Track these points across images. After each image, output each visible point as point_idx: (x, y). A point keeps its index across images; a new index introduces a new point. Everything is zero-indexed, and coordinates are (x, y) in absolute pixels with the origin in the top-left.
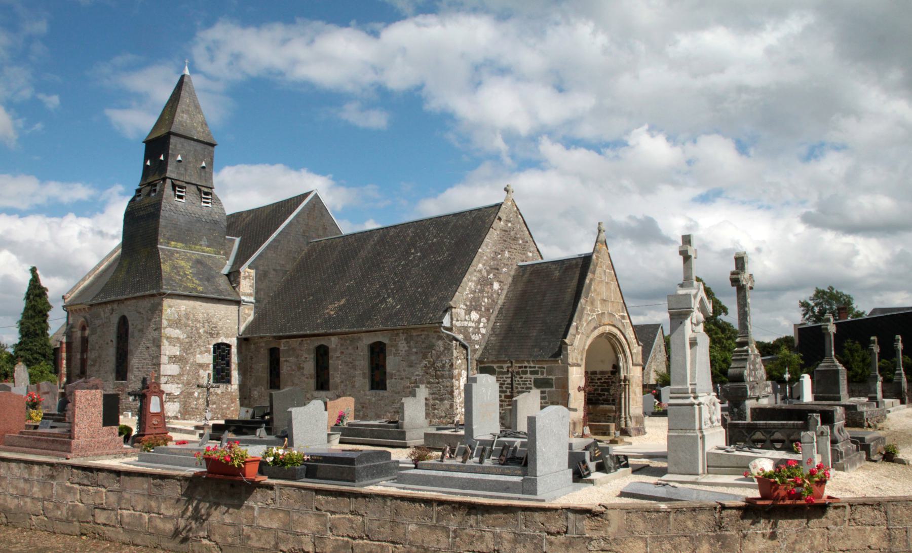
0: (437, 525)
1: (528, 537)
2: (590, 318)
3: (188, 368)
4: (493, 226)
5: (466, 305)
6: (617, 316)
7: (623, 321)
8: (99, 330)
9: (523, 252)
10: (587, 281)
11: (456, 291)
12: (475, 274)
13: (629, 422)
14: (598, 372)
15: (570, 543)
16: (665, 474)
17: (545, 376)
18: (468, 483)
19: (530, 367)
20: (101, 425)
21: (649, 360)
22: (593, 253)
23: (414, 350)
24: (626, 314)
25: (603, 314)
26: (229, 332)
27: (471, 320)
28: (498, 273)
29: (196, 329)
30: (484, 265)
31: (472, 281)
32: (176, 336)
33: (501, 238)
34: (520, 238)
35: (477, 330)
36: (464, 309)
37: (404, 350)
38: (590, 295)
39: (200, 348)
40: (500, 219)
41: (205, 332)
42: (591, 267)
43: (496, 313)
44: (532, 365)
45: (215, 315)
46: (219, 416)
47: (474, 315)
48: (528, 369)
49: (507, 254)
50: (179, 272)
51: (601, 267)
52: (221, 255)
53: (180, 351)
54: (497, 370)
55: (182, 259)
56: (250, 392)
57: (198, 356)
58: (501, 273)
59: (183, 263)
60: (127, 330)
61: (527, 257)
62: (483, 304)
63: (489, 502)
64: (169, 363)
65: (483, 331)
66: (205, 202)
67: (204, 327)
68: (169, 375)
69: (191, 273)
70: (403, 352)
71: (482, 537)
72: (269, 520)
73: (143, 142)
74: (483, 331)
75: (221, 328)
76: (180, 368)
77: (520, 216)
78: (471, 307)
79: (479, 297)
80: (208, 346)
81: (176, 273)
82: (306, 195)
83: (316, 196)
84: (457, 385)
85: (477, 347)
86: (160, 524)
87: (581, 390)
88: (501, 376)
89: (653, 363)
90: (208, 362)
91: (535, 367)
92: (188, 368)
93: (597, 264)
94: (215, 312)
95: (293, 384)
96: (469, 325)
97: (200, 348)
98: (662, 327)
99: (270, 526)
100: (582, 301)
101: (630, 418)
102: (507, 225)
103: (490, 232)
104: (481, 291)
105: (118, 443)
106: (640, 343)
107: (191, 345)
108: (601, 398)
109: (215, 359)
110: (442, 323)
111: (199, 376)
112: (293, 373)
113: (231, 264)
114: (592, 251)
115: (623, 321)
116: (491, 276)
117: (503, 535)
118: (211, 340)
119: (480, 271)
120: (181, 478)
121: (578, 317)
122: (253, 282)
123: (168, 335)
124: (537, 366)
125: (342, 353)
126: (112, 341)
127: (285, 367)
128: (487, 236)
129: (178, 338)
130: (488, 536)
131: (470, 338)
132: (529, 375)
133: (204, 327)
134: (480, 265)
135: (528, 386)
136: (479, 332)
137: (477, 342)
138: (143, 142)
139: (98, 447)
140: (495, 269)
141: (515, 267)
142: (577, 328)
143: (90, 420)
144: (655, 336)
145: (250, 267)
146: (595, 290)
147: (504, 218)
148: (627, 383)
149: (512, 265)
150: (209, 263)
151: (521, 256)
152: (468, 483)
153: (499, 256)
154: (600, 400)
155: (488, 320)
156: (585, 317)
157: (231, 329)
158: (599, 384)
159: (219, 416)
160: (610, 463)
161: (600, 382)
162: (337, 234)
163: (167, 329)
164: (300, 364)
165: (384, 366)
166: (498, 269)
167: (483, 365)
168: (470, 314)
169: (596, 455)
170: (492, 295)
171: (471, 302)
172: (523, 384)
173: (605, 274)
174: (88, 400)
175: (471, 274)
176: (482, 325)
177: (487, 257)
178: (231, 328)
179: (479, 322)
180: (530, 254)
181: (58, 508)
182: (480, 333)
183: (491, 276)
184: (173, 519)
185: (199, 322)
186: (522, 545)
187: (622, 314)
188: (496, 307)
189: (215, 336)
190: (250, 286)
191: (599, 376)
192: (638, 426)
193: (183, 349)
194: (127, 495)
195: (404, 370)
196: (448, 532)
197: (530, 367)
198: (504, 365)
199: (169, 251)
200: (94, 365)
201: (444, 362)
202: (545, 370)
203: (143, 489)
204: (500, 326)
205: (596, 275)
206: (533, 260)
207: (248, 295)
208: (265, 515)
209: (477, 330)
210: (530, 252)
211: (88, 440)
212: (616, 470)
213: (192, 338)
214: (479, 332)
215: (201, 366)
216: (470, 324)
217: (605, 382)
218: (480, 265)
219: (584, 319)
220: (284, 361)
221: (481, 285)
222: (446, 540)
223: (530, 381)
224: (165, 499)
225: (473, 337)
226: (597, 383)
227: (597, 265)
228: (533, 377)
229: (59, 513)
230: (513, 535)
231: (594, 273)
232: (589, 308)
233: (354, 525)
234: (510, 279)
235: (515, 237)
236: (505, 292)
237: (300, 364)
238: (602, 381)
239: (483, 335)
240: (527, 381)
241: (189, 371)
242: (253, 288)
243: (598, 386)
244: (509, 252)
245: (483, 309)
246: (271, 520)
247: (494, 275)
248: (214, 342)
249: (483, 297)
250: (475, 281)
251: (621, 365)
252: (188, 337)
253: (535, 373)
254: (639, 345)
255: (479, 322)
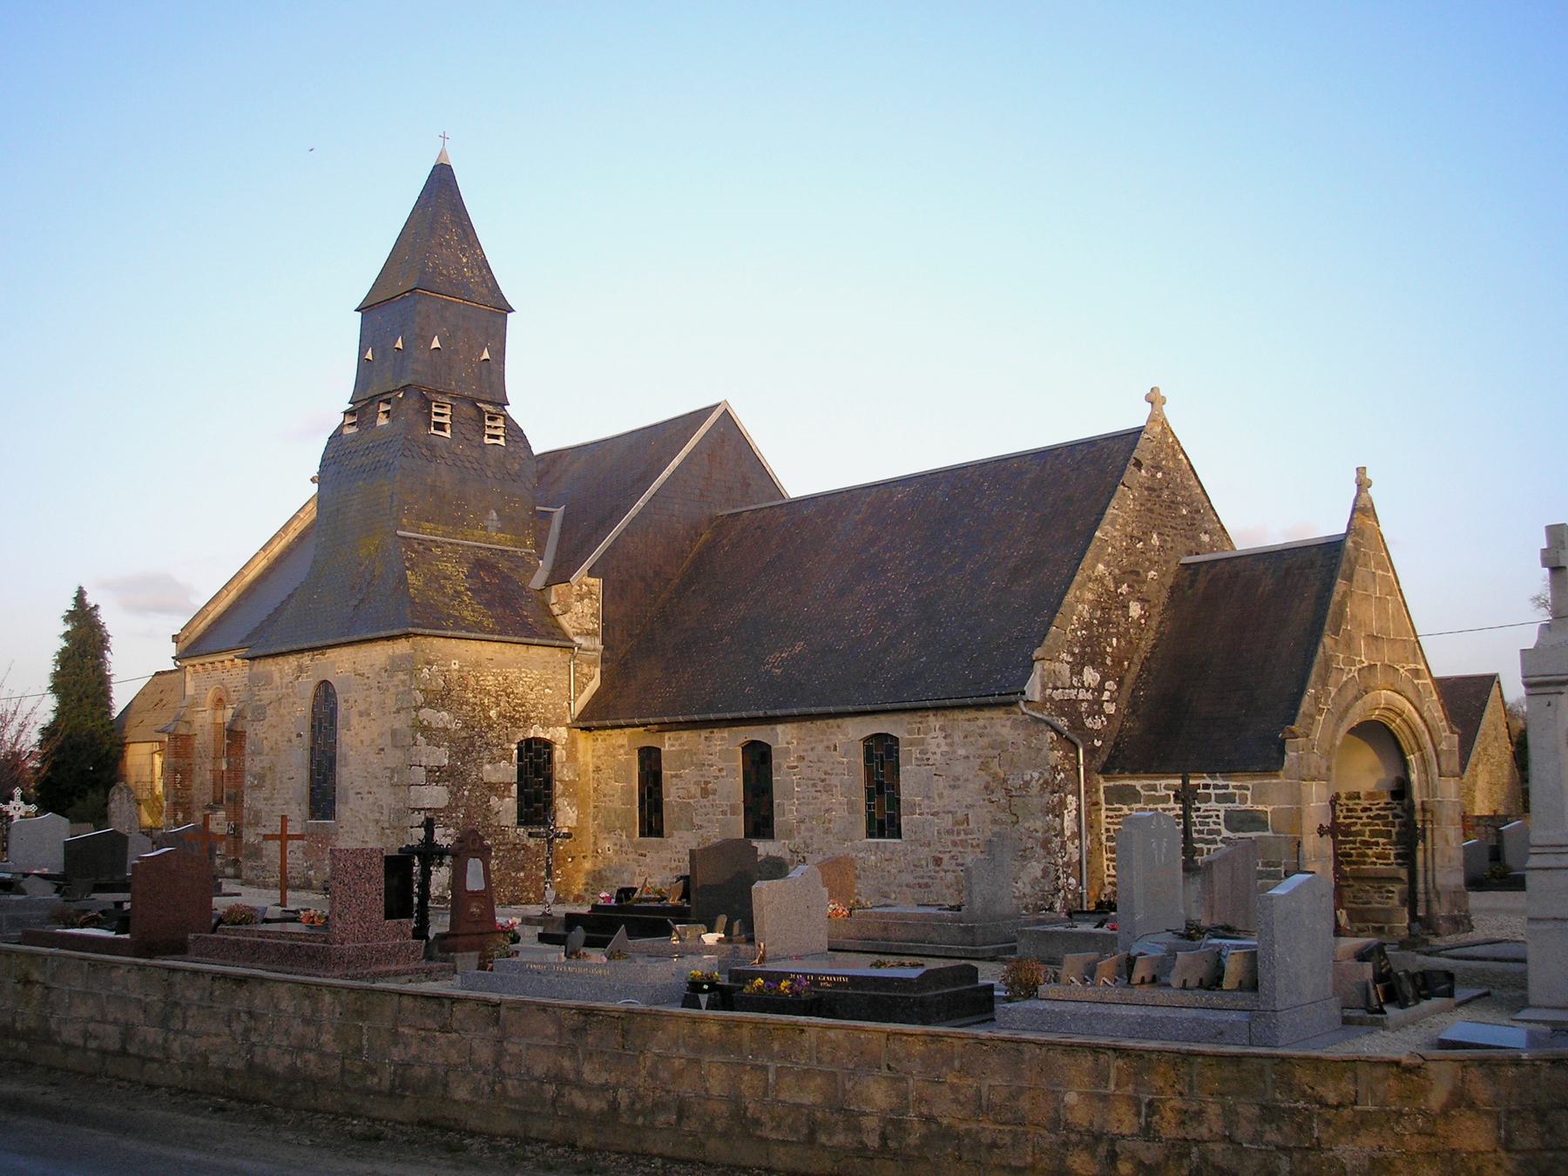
0: (1117, 1092)
1: (1284, 1112)
2: (1345, 679)
3: (466, 793)
4: (1124, 479)
5: (1073, 654)
6: (1402, 670)
7: (1416, 682)
8: (269, 712)
9: (1190, 533)
10: (1336, 597)
11: (1050, 624)
12: (1090, 585)
13: (1436, 907)
14: (1362, 795)
15: (1362, 1122)
16: (1523, 1007)
17: (1248, 805)
18: (1140, 1024)
19: (1216, 787)
20: (382, 916)
21: (1473, 759)
22: (1346, 535)
23: (962, 752)
24: (1422, 667)
25: (1372, 667)
26: (549, 715)
27: (1083, 686)
28: (1137, 582)
29: (483, 710)
30: (1107, 565)
31: (1083, 602)
32: (441, 725)
33: (1141, 505)
34: (1183, 503)
35: (1096, 707)
36: (1068, 663)
37: (938, 751)
38: (1343, 627)
39: (490, 750)
40: (1138, 464)
41: (500, 715)
42: (1344, 566)
43: (1136, 669)
44: (1220, 782)
45: (521, 679)
46: (531, 895)
47: (1091, 676)
48: (1211, 791)
49: (1155, 540)
50: (443, 587)
51: (1366, 565)
52: (526, 547)
53: (450, 757)
54: (1142, 792)
55: (449, 560)
56: (595, 843)
57: (488, 767)
58: (1144, 582)
59: (449, 568)
60: (334, 711)
61: (1200, 544)
62: (1108, 649)
63: (1215, 1050)
64: (428, 782)
65: (1110, 708)
66: (491, 436)
67: (498, 705)
68: (430, 809)
69: (468, 589)
70: (938, 756)
71: (1201, 1112)
72: (796, 1090)
73: (357, 310)
74: (1110, 708)
75: (534, 705)
76: (451, 792)
77: (1181, 456)
78: (1082, 658)
79: (1099, 636)
80: (506, 746)
81: (436, 590)
82: (699, 416)
83: (727, 417)
84: (1058, 828)
85: (1098, 743)
86: (580, 1101)
87: (1326, 833)
88: (1151, 806)
89: (1480, 767)
90: (507, 780)
91: (1226, 787)
92: (466, 793)
93: (1356, 558)
94: (521, 672)
95: (693, 825)
96: (1080, 697)
97: (490, 750)
98: (1499, 682)
99: (798, 1101)
100: (1327, 640)
101: (1438, 894)
102: (1153, 475)
103: (1118, 494)
104: (1104, 622)
105: (412, 953)
106: (1455, 729)
107: (473, 745)
108: (1370, 852)
109: (521, 772)
110: (1023, 693)
111: (488, 809)
112: (691, 801)
113: (549, 566)
114: (1344, 531)
115: (1416, 682)
116: (1124, 588)
117: (1240, 1109)
118: (514, 734)
119: (1100, 580)
120: (623, 1015)
121: (1319, 676)
122: (599, 605)
123: (425, 723)
124: (1232, 783)
125: (802, 758)
126: (299, 735)
127: (673, 790)
128: (1113, 502)
129: (446, 729)
130: (1213, 1110)
131: (1084, 724)
132: (1213, 804)
133: (498, 705)
134: (1101, 567)
135: (1213, 827)
136: (1101, 712)
137: (1098, 734)
138: (357, 310)
139: (377, 959)
140: (1132, 572)
141: (1173, 567)
142: (1317, 699)
143: (362, 908)
144: (1485, 704)
145: (591, 573)
146: (1354, 616)
147: (1146, 462)
148: (1429, 815)
149: (1166, 562)
150: (503, 565)
151: (1187, 542)
152: (1140, 1024)
153: (1140, 545)
154: (1367, 856)
155: (1120, 684)
156: (1334, 675)
157: (555, 709)
158: (1365, 820)
159: (531, 895)
160: (1408, 989)
161: (1368, 817)
162: (773, 498)
163: (422, 711)
164: (707, 783)
165: (895, 786)
166: (1138, 574)
167: (1111, 784)
168: (1080, 673)
169: (1384, 970)
170: (1127, 630)
171: (1083, 647)
172: (1201, 824)
173: (1374, 580)
174: (358, 867)
175: (1081, 586)
176: (1106, 695)
177: (1113, 548)
178: (554, 704)
179: (1100, 688)
180: (1205, 538)
181: (373, 1072)
182: (1104, 713)
183: (1124, 588)
184: (608, 1090)
185: (488, 693)
186: (1274, 1126)
187: (1412, 666)
188: (1136, 657)
189: (521, 724)
190: (592, 615)
191: (1366, 804)
192: (1456, 913)
193: (456, 753)
194: (512, 1048)
195: (941, 796)
196: (1138, 1106)
197: (1216, 787)
198: (1158, 783)
199: (421, 542)
200: (260, 787)
201: (1027, 778)
202: (1249, 793)
203: (546, 1036)
204: (1145, 696)
205: (1355, 584)
206: (1212, 551)
207: (588, 634)
208: (790, 1080)
209: (1096, 708)
210: (1206, 533)
211: (359, 945)
212: (1417, 1002)
213: (474, 728)
214: (1101, 712)
215: (492, 787)
216: (1083, 695)
217: (1377, 817)
218: (1101, 567)
219: (1331, 680)
220: (672, 776)
221: (1103, 609)
222: (1135, 1120)
223: (1217, 816)
224: (591, 1054)
225: (1089, 723)
226: (1361, 818)
227: (1356, 562)
228: (1223, 807)
229: (376, 1080)
230: (1257, 1107)
231: (1349, 578)
232: (1341, 656)
233: (961, 1097)
234: (1165, 594)
235: (1173, 502)
236: (1154, 624)
237: (707, 783)
238: (1372, 814)
239: (1109, 717)
240: (1211, 817)
241: (468, 798)
242: (598, 618)
243: (1363, 825)
244: (1159, 534)
245: (1108, 661)
246: (801, 1089)
247: (1129, 586)
248: (520, 737)
249: (1111, 635)
250: (1090, 602)
251: (1414, 777)
252: (466, 726)
253: (1228, 798)
254: (1453, 732)
255: (1100, 688)
